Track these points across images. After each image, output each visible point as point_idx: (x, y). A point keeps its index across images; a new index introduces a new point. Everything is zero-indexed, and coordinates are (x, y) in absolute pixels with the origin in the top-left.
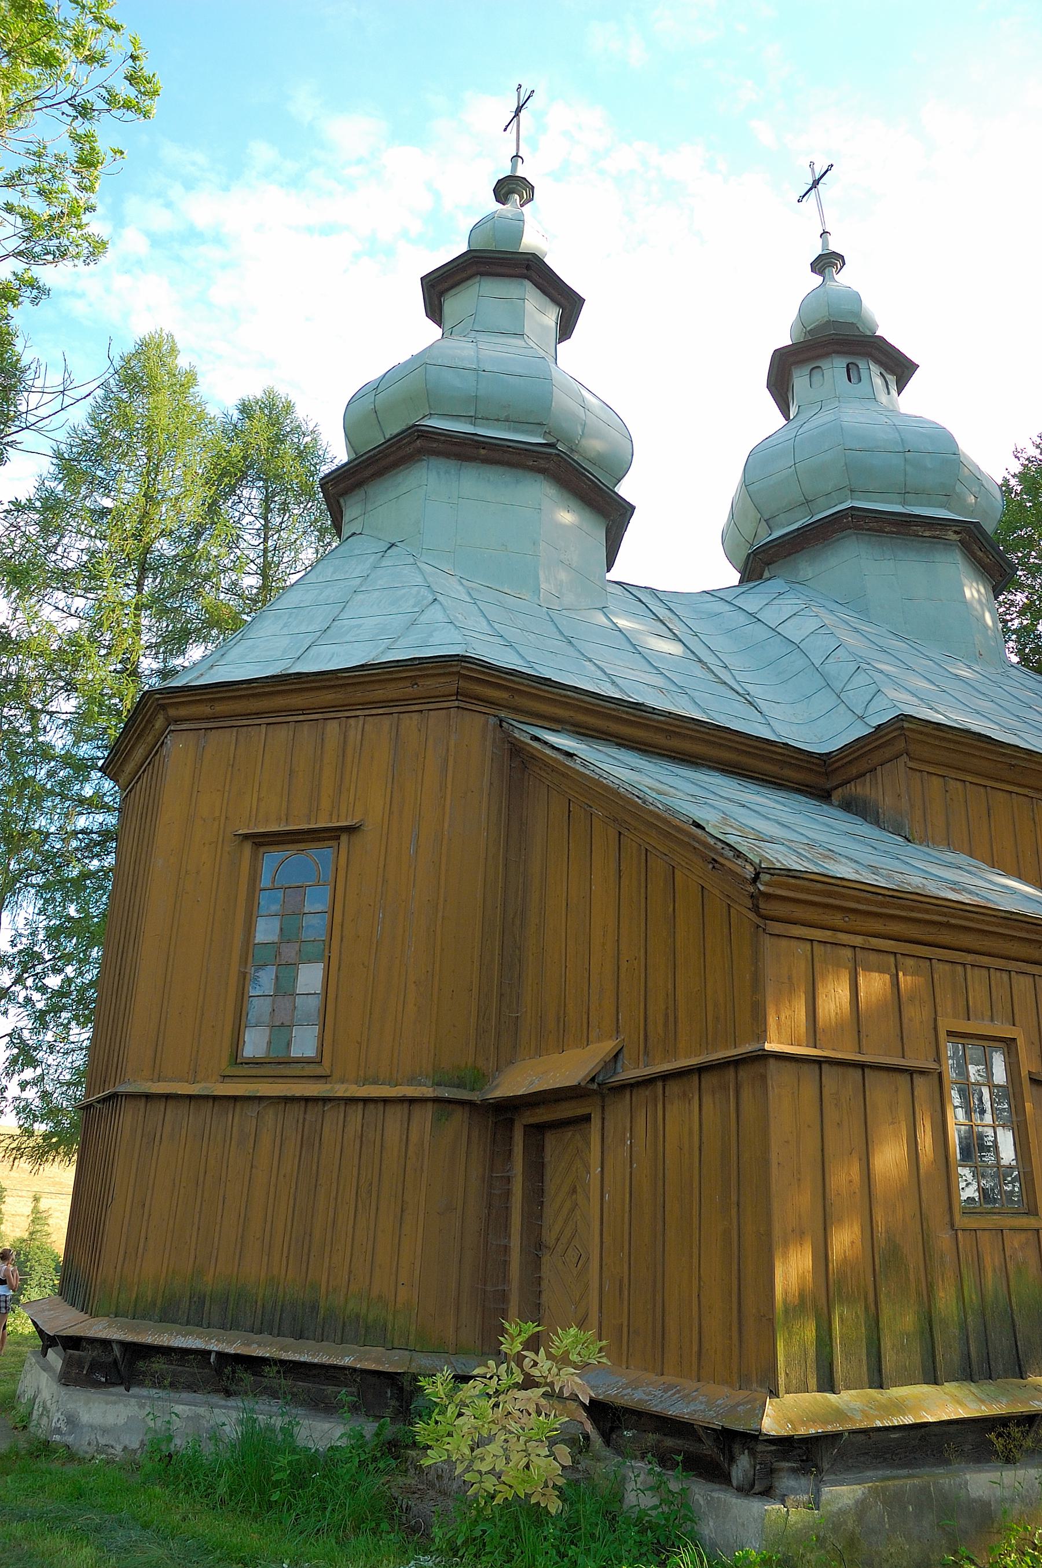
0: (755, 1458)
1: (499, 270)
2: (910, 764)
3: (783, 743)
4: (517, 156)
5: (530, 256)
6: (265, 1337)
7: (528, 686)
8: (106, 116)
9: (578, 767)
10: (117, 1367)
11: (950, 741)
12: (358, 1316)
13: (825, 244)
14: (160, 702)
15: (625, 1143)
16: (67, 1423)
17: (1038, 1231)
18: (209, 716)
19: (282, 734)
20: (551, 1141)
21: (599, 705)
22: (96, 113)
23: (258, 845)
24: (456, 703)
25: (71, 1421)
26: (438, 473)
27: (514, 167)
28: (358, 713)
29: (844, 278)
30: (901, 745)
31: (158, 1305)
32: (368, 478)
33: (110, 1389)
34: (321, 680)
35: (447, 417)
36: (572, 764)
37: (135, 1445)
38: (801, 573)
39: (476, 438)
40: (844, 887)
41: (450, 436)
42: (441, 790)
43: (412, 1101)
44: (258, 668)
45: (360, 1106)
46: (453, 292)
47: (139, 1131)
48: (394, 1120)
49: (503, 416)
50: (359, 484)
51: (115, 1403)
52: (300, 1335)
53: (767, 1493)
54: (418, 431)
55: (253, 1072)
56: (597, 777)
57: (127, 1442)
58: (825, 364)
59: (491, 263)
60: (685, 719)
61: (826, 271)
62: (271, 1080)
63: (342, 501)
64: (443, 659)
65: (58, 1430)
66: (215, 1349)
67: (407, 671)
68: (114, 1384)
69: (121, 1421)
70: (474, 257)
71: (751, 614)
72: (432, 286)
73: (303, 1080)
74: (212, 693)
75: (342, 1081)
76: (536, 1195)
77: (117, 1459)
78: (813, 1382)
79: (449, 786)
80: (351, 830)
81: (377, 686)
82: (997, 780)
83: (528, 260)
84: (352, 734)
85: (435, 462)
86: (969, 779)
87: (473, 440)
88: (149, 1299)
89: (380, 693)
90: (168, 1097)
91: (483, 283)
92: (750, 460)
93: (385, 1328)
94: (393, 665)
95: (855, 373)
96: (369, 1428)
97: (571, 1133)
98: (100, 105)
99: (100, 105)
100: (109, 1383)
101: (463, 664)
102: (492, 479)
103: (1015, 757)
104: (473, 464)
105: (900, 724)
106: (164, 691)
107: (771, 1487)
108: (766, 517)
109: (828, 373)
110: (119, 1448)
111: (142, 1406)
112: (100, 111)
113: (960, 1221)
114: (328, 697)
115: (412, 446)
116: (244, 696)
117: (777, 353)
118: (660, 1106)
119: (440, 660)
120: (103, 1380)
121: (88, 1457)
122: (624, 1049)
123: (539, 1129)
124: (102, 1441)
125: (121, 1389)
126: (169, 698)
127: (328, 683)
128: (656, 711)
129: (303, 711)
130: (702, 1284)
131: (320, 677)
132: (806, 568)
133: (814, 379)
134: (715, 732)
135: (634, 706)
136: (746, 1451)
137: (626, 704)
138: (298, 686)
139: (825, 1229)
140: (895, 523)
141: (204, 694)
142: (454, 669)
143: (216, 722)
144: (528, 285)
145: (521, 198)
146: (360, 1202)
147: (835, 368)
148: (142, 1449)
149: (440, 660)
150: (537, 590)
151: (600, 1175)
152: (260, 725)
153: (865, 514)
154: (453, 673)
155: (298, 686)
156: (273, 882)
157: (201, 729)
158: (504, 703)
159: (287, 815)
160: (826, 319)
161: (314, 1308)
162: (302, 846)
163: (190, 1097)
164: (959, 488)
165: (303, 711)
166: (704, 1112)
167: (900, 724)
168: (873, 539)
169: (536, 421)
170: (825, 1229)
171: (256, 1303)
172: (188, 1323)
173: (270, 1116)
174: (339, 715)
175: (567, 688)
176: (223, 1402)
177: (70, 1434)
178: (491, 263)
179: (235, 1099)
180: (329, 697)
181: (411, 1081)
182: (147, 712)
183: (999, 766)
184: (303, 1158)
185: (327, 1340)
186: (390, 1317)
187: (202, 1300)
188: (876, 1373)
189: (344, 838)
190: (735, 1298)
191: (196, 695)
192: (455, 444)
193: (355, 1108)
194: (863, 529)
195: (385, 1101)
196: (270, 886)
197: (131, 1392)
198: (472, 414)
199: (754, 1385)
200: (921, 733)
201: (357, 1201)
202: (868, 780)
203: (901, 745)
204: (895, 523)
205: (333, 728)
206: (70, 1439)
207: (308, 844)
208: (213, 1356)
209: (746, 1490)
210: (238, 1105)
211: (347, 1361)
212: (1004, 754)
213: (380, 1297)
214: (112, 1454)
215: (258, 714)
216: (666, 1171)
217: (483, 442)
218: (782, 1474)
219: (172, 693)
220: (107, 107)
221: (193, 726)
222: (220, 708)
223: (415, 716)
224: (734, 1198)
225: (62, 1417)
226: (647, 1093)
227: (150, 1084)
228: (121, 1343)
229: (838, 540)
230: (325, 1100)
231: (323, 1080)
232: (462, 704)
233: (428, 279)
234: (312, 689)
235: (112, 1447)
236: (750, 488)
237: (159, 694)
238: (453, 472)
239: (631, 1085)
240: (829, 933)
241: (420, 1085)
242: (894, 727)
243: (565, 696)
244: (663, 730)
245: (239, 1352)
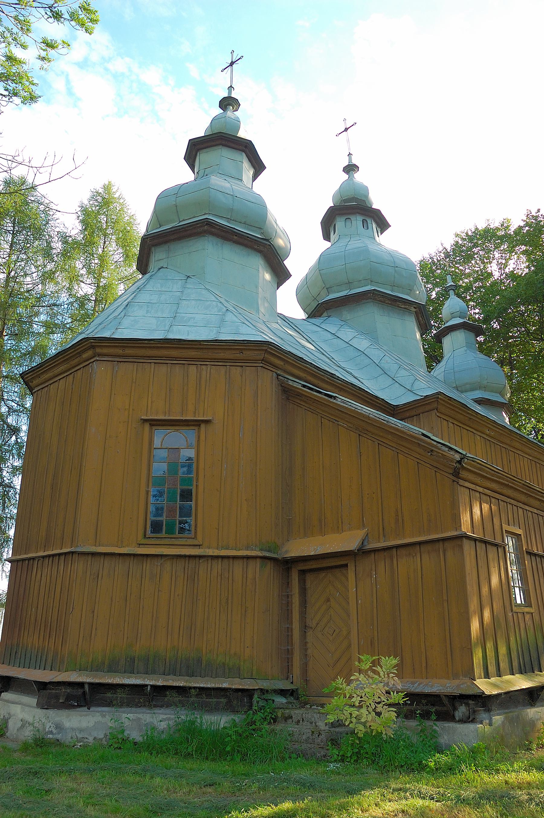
0: (469, 707)
1: (233, 145)
2: (438, 414)
3: (382, 399)
4: (231, 86)
5: (249, 142)
6: (171, 677)
7: (292, 360)
8: (66, 23)
9: (339, 403)
10: (85, 696)
11: (453, 405)
12: (224, 664)
13: (350, 160)
14: (93, 344)
15: (371, 577)
16: (56, 728)
17: (532, 613)
18: (121, 355)
19: (163, 369)
20: (310, 578)
21: (317, 373)
22: (63, 19)
23: (151, 425)
24: (261, 365)
25: (59, 727)
26: (213, 244)
27: (230, 92)
28: (208, 363)
29: (358, 177)
30: (435, 405)
31: (106, 663)
32: (172, 240)
33: (77, 709)
34: (191, 345)
35: (216, 216)
36: (334, 401)
37: (101, 736)
38: (344, 316)
39: (235, 230)
40: (486, 467)
41: (221, 227)
42: (254, 407)
43: (248, 558)
44: (147, 333)
45: (220, 560)
46: (205, 150)
47: (88, 573)
48: (238, 568)
49: (243, 221)
50: (166, 242)
51: (86, 715)
52: (192, 675)
53: (473, 721)
54: (207, 221)
55: (158, 542)
56: (354, 409)
57: (96, 735)
58: (353, 218)
59: (229, 141)
60: (349, 384)
61: (351, 172)
62: (168, 546)
63: (153, 249)
64: (260, 343)
65: (51, 732)
66: (150, 683)
67: (239, 346)
68: (81, 706)
69: (91, 724)
70: (222, 136)
71: (333, 334)
72: (194, 145)
73: (186, 547)
74: (134, 343)
75: (209, 548)
76: (304, 603)
77: (90, 744)
78: (483, 676)
79: (259, 404)
80: (207, 422)
81: (220, 351)
82: (464, 424)
83: (247, 143)
84: (204, 373)
85: (211, 238)
86: (455, 423)
87: (232, 231)
88: (100, 660)
89: (222, 355)
90: (105, 554)
91: (223, 150)
92: (321, 258)
93: (239, 669)
94: (233, 342)
95: (366, 225)
96: (237, 718)
97: (324, 574)
98: (66, 16)
99: (66, 16)
100: (79, 706)
101: (270, 346)
102: (237, 251)
103: (472, 415)
104: (229, 243)
105: (437, 396)
106: (97, 339)
107: (474, 718)
108: (328, 287)
109: (354, 222)
110: (91, 739)
111: (103, 716)
112: (65, 19)
113: (515, 609)
114: (192, 353)
115: (201, 229)
116: (144, 347)
117: (331, 208)
118: (395, 560)
119: (259, 342)
120: (76, 704)
121: (73, 744)
122: (369, 535)
123: (303, 572)
124: (80, 736)
125: (85, 709)
126: (100, 343)
127: (194, 346)
128: (339, 379)
129: (176, 359)
130: (426, 637)
131: (190, 343)
132: (346, 314)
133: (347, 224)
134: (359, 391)
135: (331, 375)
136: (463, 705)
137: (329, 374)
138: (177, 346)
139: (481, 610)
140: (390, 300)
141: (111, 343)
142: (264, 348)
143: (124, 358)
144: (244, 154)
145: (233, 108)
146: (221, 607)
147: (357, 221)
148: (106, 738)
149: (259, 342)
150: (258, 311)
151: (355, 592)
152: (151, 363)
153: (379, 293)
154: (263, 350)
155: (177, 346)
156: (161, 445)
157: (115, 361)
158: (281, 367)
159: (169, 411)
160: (353, 196)
161: (199, 661)
162: (177, 428)
163: (120, 555)
164: (415, 288)
165: (176, 359)
166: (423, 562)
167: (437, 396)
168: (380, 305)
169: (258, 227)
170: (481, 610)
171: (165, 659)
172: (125, 672)
173: (168, 565)
174: (197, 363)
175: (308, 363)
176: (149, 711)
177: (59, 733)
178: (229, 141)
179: (147, 556)
180: (193, 353)
181: (247, 548)
182: (77, 349)
183: (466, 418)
184: (188, 586)
185: (207, 676)
186: (242, 663)
187: (133, 660)
188: (498, 672)
189: (203, 426)
190: (448, 641)
191: (115, 343)
192: (223, 231)
193: (216, 561)
194: (376, 300)
195: (234, 558)
196: (160, 447)
197: (91, 710)
198: (229, 217)
199: (461, 677)
200: (444, 401)
201: (220, 606)
202: (415, 419)
203: (435, 405)
204: (390, 300)
205: (193, 369)
206: (59, 737)
207: (180, 427)
208: (149, 688)
209: (463, 721)
210: (149, 559)
211: (225, 685)
212: (468, 413)
213: (235, 654)
214: (87, 742)
215: (150, 357)
216: (400, 588)
217: (236, 233)
218: (480, 712)
219: (101, 340)
220: (69, 18)
221: (110, 359)
222: (128, 351)
223: (239, 368)
224: (445, 598)
225: (52, 725)
226: (385, 554)
227: (94, 547)
228: (91, 684)
229: (364, 303)
230: (200, 557)
231: (198, 547)
232: (264, 366)
233: (194, 141)
234: (184, 348)
235: (87, 738)
236: (321, 272)
237: (93, 339)
238: (219, 245)
239: (375, 551)
240: (474, 486)
241: (252, 550)
242: (435, 396)
243: (306, 367)
244: (338, 387)
245: (165, 684)
